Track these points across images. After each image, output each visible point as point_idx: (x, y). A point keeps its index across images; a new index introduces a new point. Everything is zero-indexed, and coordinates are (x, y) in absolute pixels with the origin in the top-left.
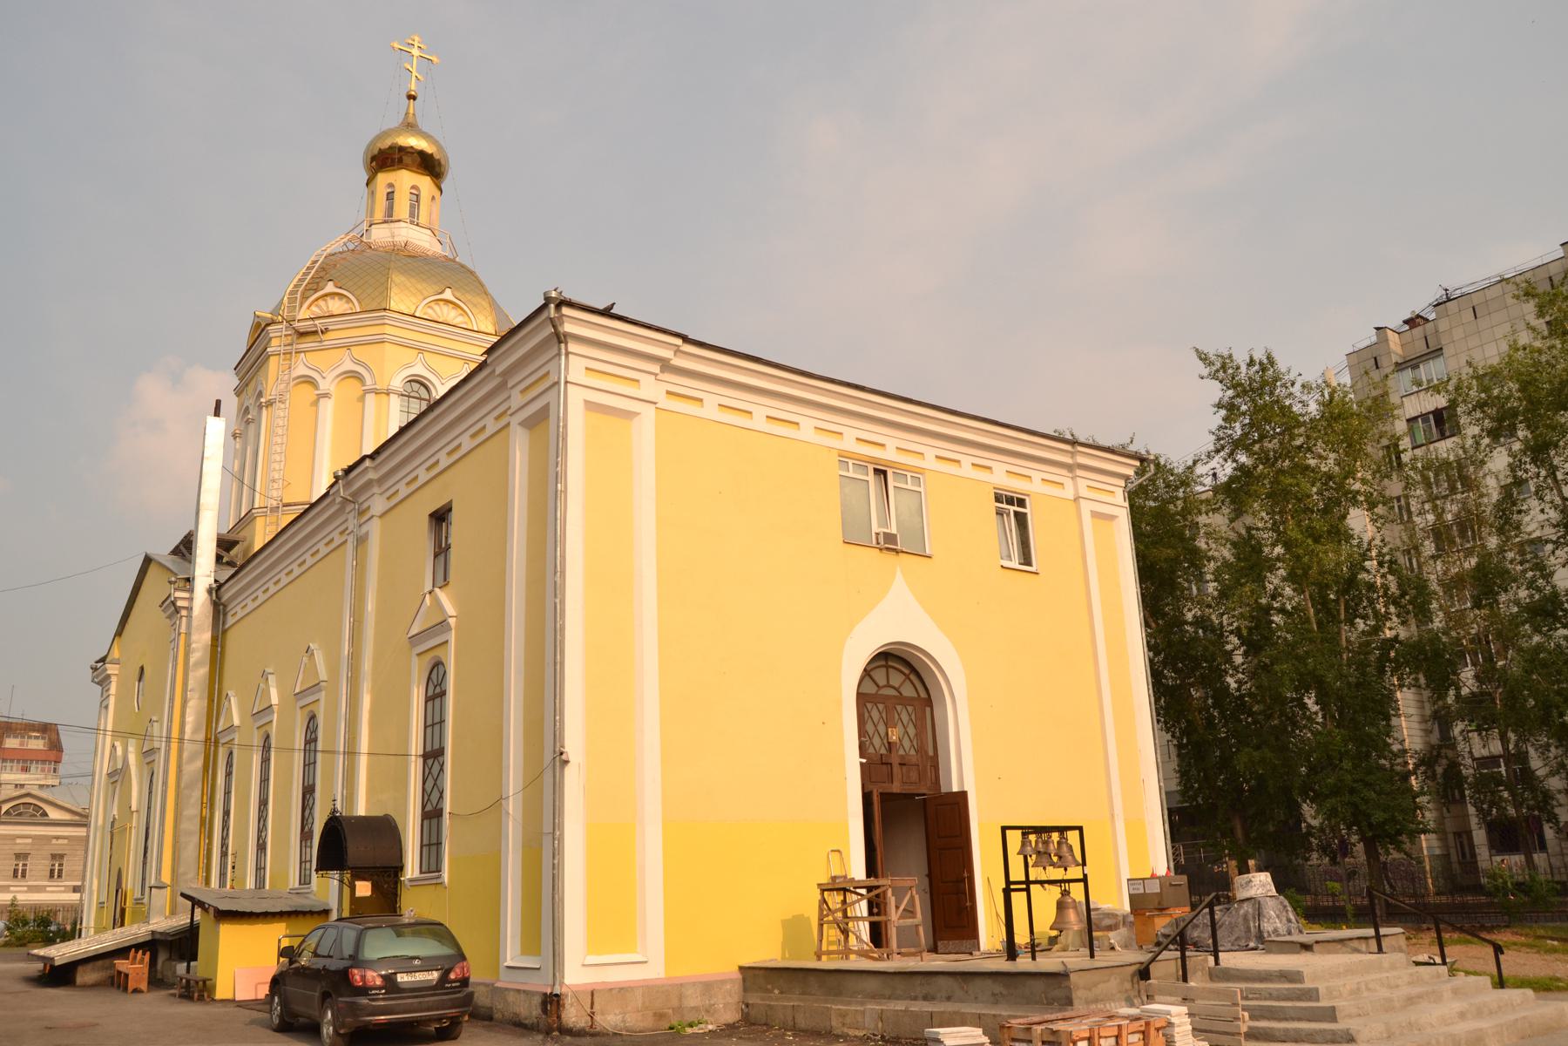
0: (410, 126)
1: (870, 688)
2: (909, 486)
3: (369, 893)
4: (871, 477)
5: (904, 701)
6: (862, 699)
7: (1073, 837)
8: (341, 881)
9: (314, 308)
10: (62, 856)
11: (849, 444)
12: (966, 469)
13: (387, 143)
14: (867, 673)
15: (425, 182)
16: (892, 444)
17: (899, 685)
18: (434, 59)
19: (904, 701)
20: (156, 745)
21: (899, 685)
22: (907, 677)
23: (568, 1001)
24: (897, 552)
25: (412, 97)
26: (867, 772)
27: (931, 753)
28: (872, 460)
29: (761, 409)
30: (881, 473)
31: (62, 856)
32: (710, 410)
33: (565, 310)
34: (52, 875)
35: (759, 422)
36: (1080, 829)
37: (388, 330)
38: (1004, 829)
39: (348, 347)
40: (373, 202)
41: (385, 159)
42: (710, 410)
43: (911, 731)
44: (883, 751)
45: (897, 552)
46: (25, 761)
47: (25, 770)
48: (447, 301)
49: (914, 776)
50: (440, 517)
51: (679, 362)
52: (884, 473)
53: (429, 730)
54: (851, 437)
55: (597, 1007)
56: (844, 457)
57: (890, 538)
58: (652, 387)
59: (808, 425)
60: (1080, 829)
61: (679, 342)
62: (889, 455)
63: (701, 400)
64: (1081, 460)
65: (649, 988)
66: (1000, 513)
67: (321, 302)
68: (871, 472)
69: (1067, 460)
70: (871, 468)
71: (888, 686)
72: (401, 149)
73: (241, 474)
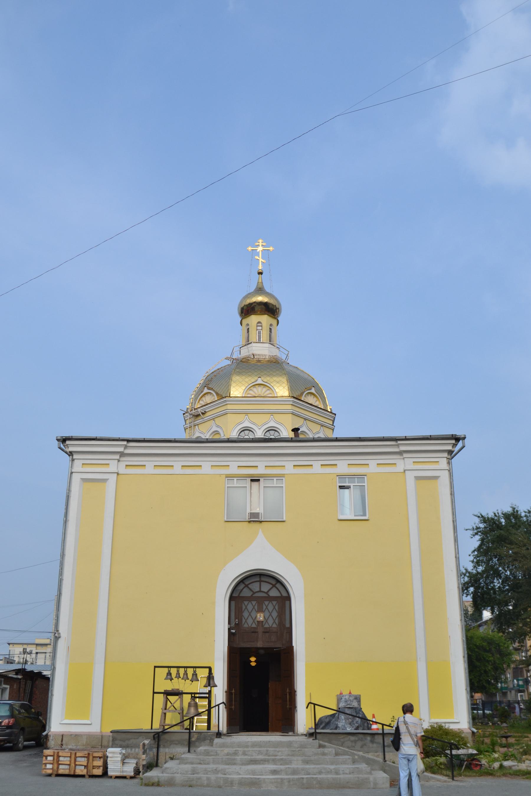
0: (260, 290)
5: (271, 599)
9: (201, 402)
13: (248, 301)
15: (265, 319)
18: (271, 248)
19: (271, 599)
23: (51, 738)
24: (261, 522)
25: (260, 273)
26: (231, 636)
29: (177, 464)
33: (68, 442)
37: (229, 407)
38: (155, 667)
39: (213, 419)
41: (247, 311)
43: (275, 614)
45: (261, 522)
48: (260, 385)
51: (128, 451)
54: (234, 466)
55: (64, 742)
58: (113, 466)
59: (207, 466)
61: (125, 443)
62: (261, 470)
64: (403, 448)
65: (90, 736)
67: (203, 398)
69: (396, 450)
70: (249, 480)
71: (260, 591)
72: (251, 304)
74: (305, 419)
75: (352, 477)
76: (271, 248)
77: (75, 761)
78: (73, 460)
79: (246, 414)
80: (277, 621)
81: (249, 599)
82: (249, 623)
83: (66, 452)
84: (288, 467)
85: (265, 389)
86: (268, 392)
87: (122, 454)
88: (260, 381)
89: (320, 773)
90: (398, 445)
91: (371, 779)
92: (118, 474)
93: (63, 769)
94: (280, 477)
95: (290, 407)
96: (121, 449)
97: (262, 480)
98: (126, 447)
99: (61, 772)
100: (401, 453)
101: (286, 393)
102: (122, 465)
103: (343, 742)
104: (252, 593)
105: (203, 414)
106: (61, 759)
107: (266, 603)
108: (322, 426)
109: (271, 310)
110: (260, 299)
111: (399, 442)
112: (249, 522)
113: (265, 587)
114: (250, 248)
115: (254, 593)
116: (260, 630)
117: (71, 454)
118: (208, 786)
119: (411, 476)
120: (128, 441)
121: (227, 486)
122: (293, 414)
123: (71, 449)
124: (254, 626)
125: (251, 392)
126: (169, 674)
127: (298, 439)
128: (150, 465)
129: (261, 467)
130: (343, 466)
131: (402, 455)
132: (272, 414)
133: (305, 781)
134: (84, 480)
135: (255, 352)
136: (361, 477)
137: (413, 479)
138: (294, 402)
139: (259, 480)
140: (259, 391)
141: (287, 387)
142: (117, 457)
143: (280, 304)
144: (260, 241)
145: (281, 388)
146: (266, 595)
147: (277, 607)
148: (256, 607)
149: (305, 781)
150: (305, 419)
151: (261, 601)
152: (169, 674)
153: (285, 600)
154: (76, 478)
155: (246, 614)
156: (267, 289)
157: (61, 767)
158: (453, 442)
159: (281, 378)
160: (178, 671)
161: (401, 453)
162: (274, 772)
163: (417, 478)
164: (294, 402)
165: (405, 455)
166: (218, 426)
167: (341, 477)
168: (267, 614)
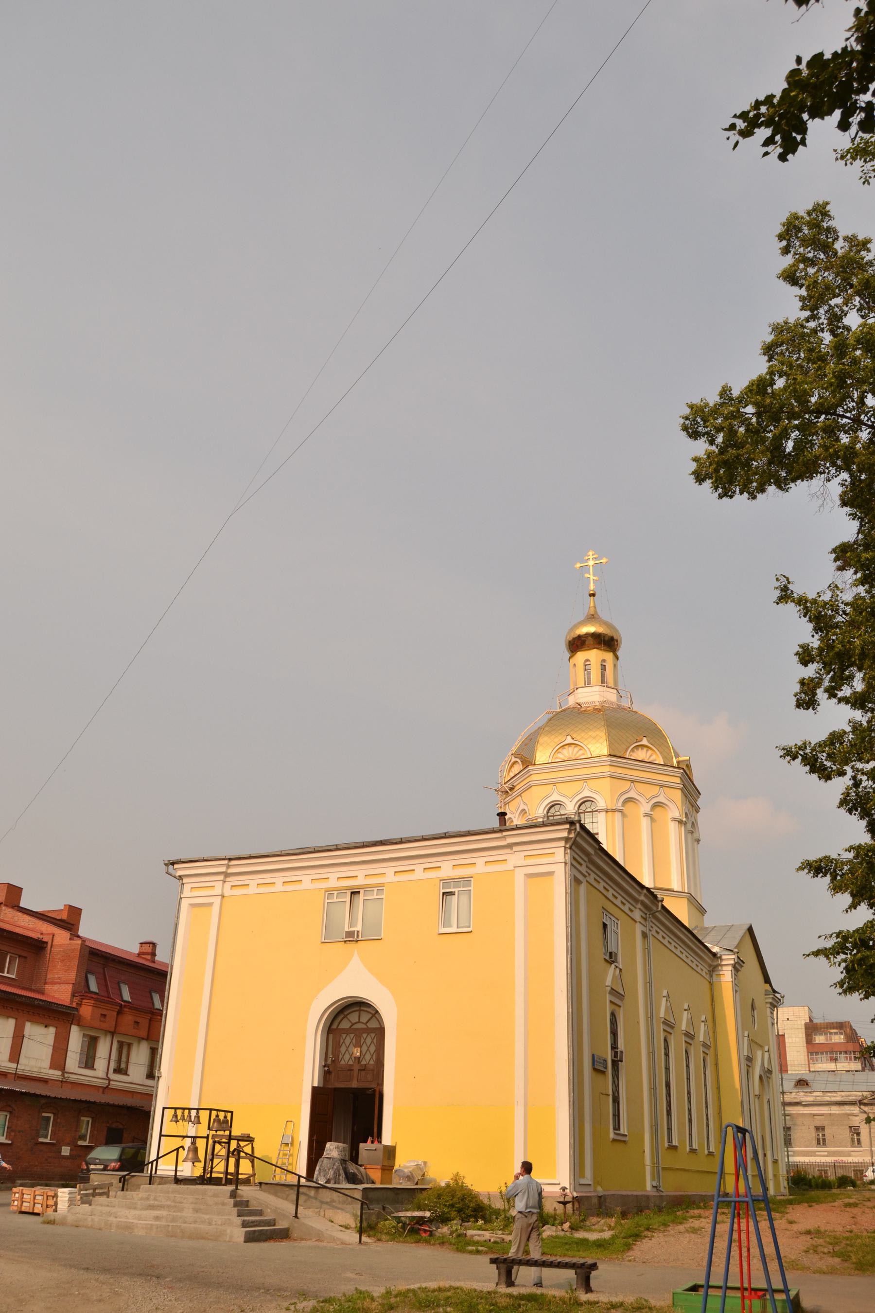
0: (592, 618)
3: (328, 1145)
7: (229, 1115)
10: (823, 1128)
11: (333, 883)
12: (419, 873)
17: (352, 1024)
21: (352, 1024)
22: (345, 1016)
25: (593, 595)
29: (279, 879)
31: (823, 1128)
32: (253, 889)
33: (176, 866)
34: (819, 1143)
35: (279, 887)
36: (232, 1112)
37: (534, 778)
41: (577, 644)
42: (253, 889)
46: (832, 1052)
47: (835, 1060)
49: (369, 1077)
51: (230, 871)
54: (334, 879)
56: (329, 892)
57: (350, 934)
59: (307, 880)
60: (232, 1112)
61: (226, 862)
62: (360, 881)
64: (510, 840)
71: (359, 1022)
72: (579, 637)
74: (633, 781)
75: (457, 881)
76: (604, 560)
77: (35, 1198)
78: (183, 884)
79: (554, 784)
80: (374, 1057)
81: (347, 1031)
82: (345, 1060)
83: (175, 877)
84: (388, 874)
85: (576, 749)
86: (581, 752)
87: (227, 875)
88: (569, 740)
89: (195, 1222)
90: (504, 837)
91: (228, 1231)
92: (223, 896)
93: (26, 1207)
94: (380, 887)
95: (607, 769)
96: (223, 869)
97: (362, 891)
98: (228, 866)
99: (23, 1209)
100: (510, 846)
101: (605, 751)
102: (228, 886)
103: (288, 1196)
104: (350, 1024)
105: (511, 789)
106: (25, 1196)
107: (365, 1035)
108: (661, 786)
109: (607, 642)
110: (590, 629)
111: (505, 834)
112: (345, 942)
113: (354, 1017)
114: (578, 565)
115: (353, 1024)
116: (356, 1068)
117: (181, 878)
118: (92, 1227)
119: (520, 875)
120: (230, 859)
121: (327, 901)
122: (611, 777)
123: (180, 873)
124: (351, 1062)
125: (560, 755)
126: (175, 1116)
127: (504, 828)
128: (253, 881)
129: (360, 877)
130: (447, 869)
131: (512, 849)
132: (585, 780)
133: (170, 1229)
134: (193, 905)
135: (580, 701)
136: (467, 880)
137: (523, 876)
138: (612, 761)
139: (359, 892)
140: (567, 753)
141: (605, 743)
142: (221, 877)
143: (616, 630)
144: (591, 553)
145: (598, 745)
146: (364, 1026)
147: (375, 1041)
148: (354, 1041)
149: (170, 1229)
150: (633, 781)
151: (358, 1034)
152: (175, 1116)
153: (380, 1032)
154: (185, 903)
155: (343, 1049)
156: (603, 615)
157: (25, 1204)
158: (568, 826)
159: (597, 733)
160: (175, 1113)
161: (510, 846)
162: (157, 1218)
163: (529, 876)
164: (612, 761)
165: (515, 848)
166: (525, 804)
167: (445, 881)
168: (365, 1048)
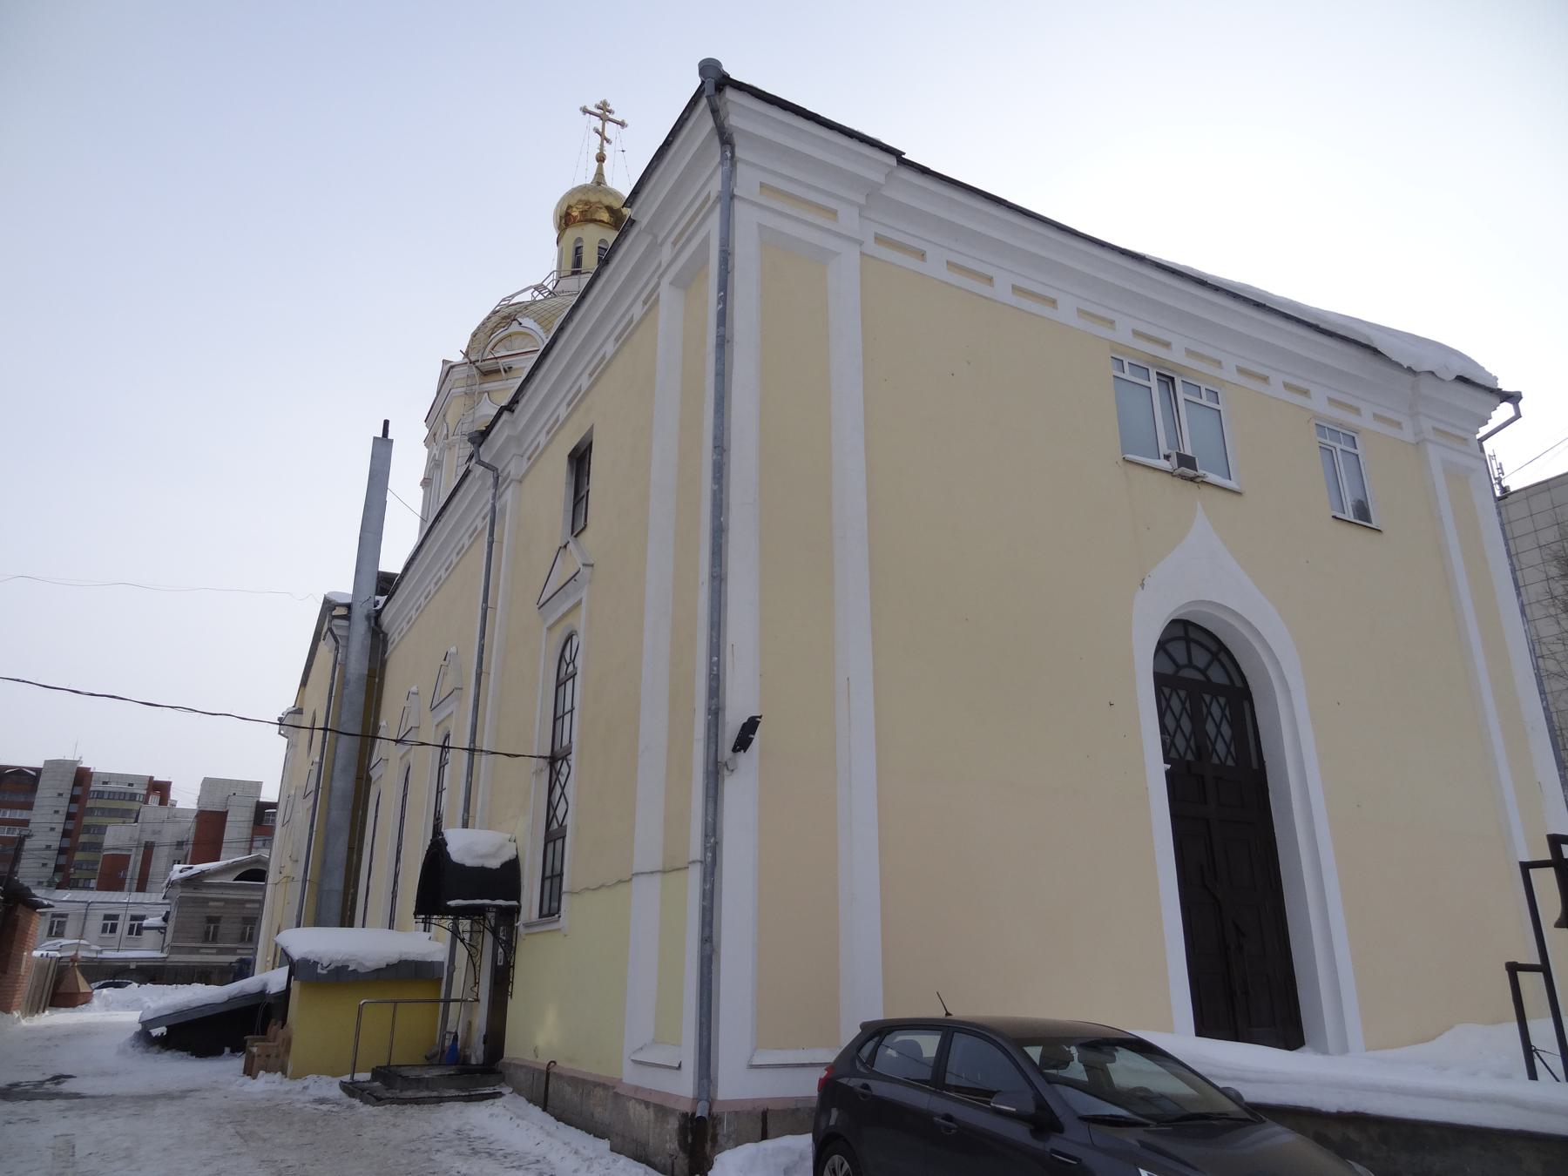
1: (1169, 669)
2: (1204, 401)
4: (1154, 383)
6: (1161, 680)
8: (455, 933)
14: (1161, 647)
16: (1277, 379)
20: (515, 362)
27: (1255, 765)
28: (1156, 361)
30: (1167, 381)
40: (722, 245)
44: (1190, 757)
50: (580, 459)
52: (1172, 379)
53: (548, 883)
62: (1176, 356)
63: (1112, 322)
66: (1327, 450)
68: (1153, 376)
71: (1190, 665)
73: (747, 163)
